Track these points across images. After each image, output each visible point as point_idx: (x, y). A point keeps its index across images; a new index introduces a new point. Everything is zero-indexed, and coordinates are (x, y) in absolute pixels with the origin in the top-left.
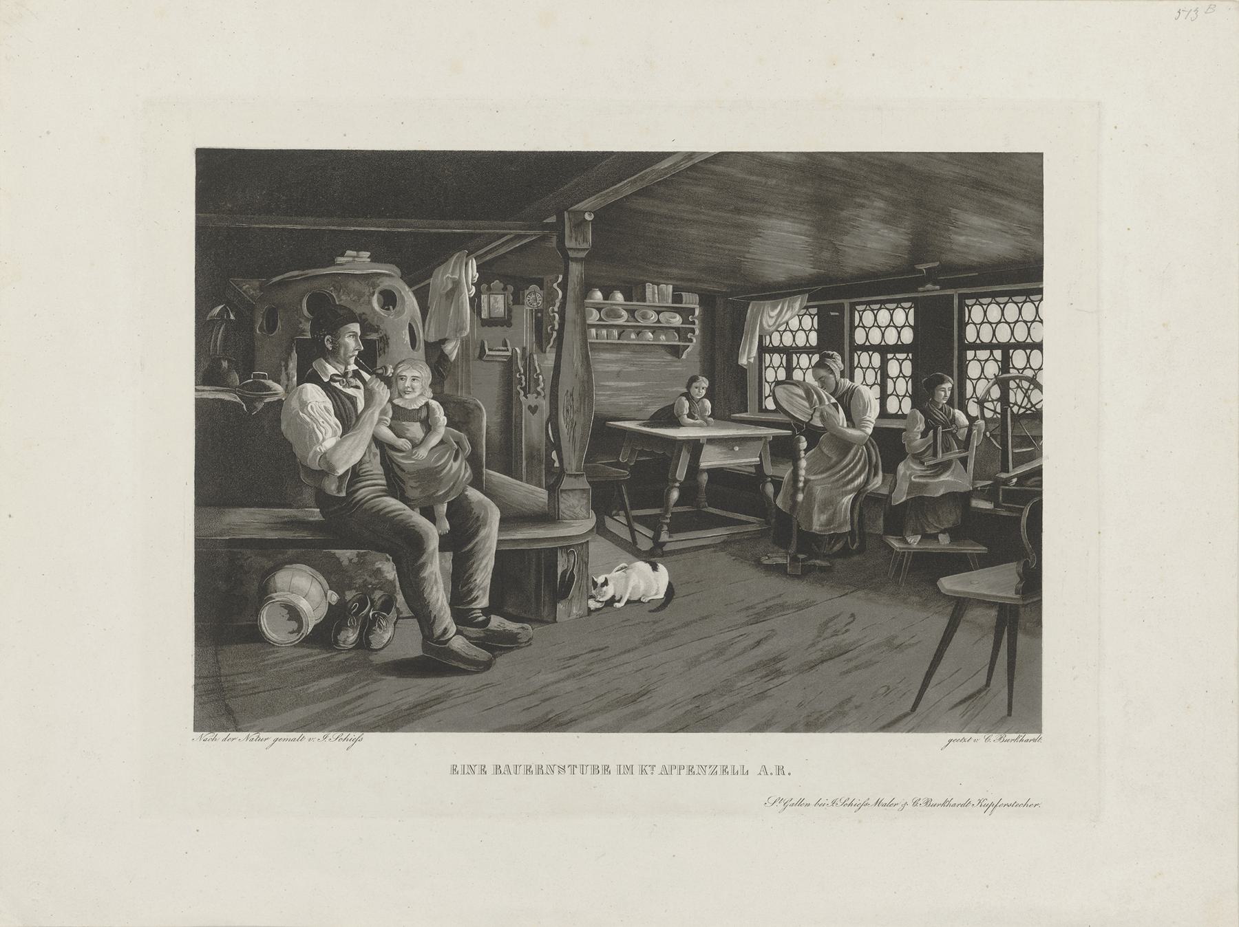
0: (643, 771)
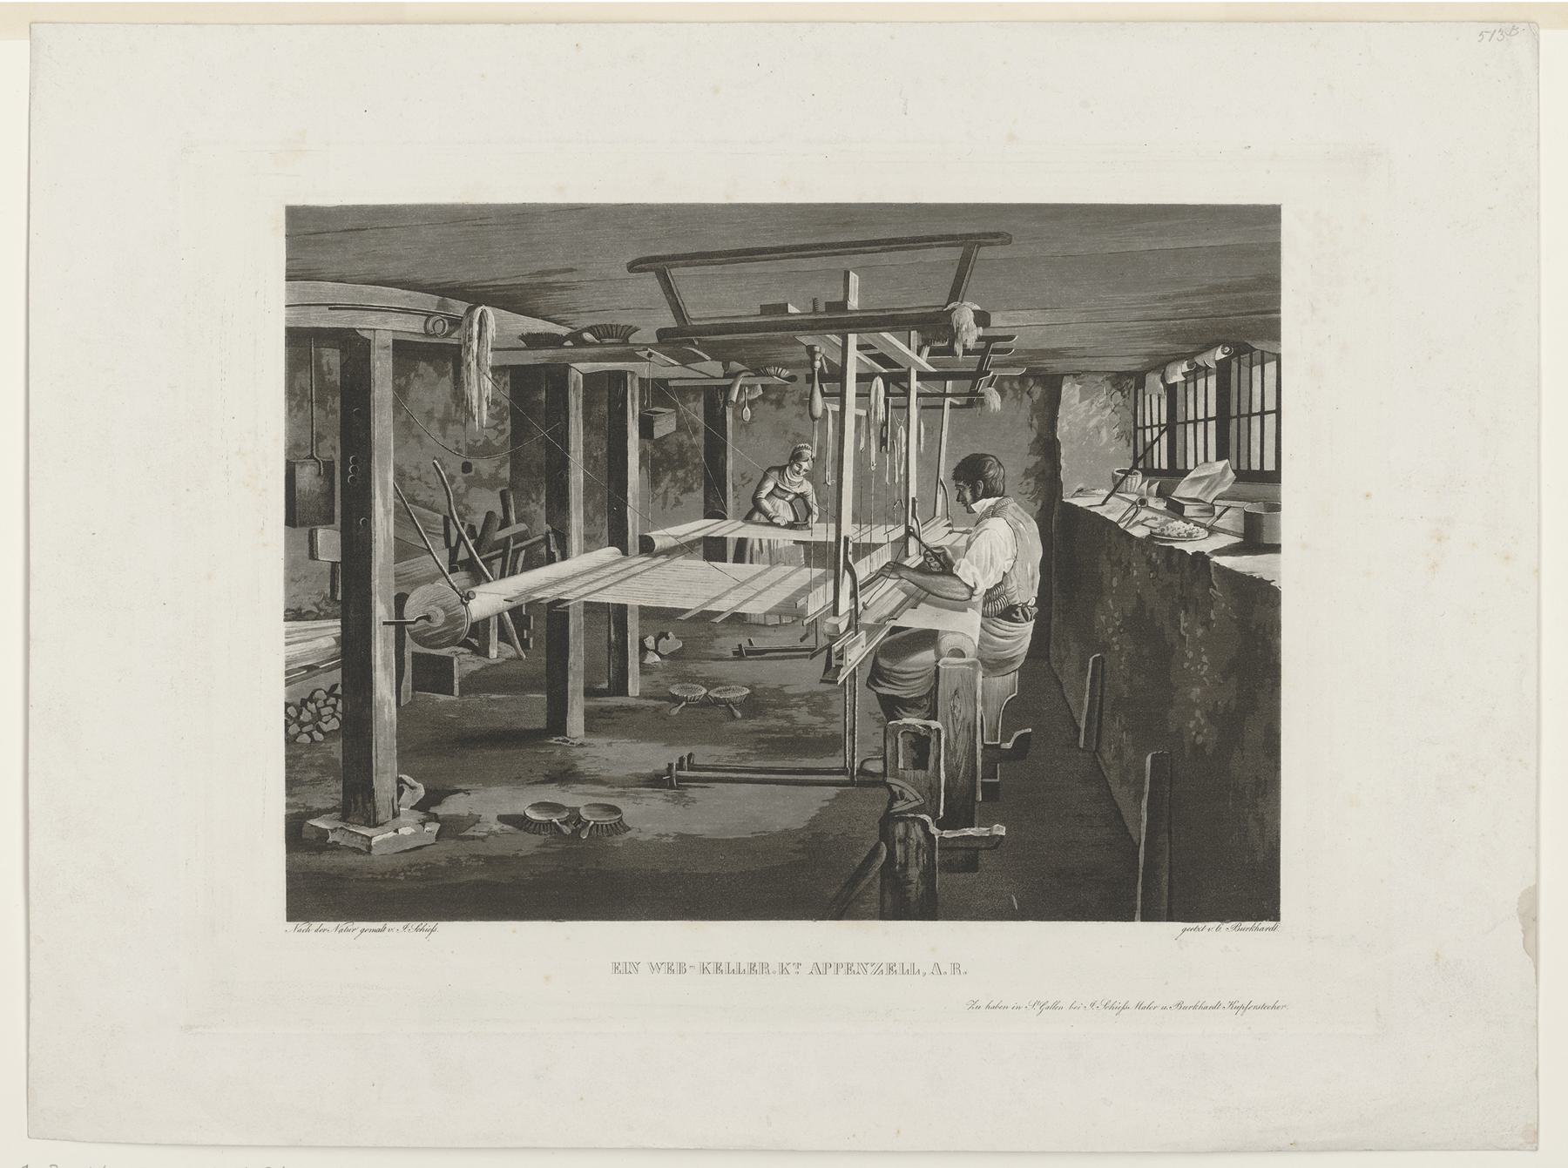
0: (783, 970)
